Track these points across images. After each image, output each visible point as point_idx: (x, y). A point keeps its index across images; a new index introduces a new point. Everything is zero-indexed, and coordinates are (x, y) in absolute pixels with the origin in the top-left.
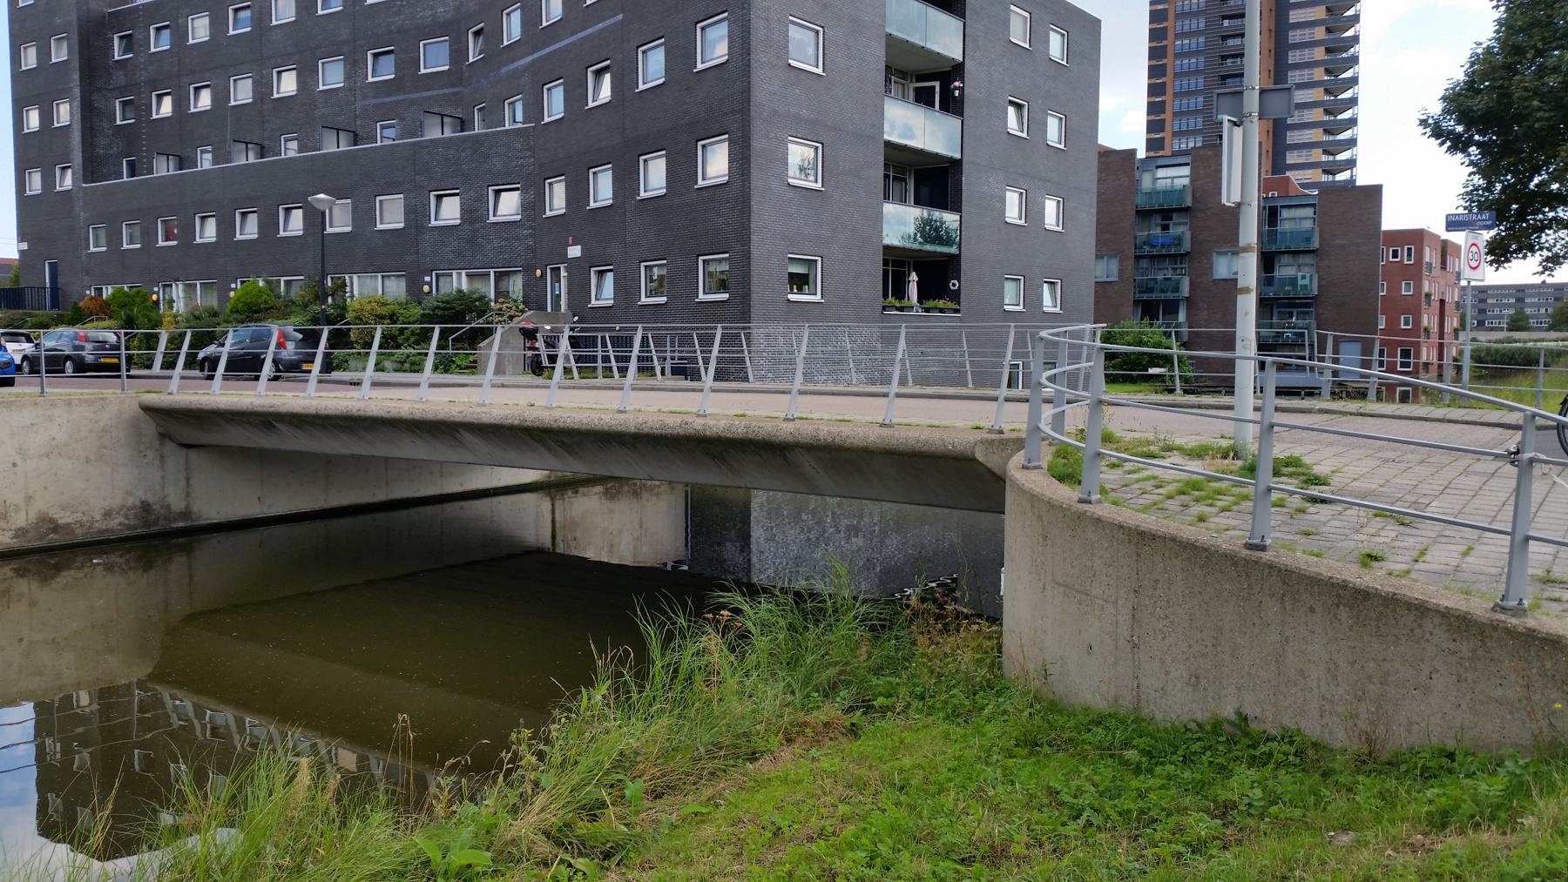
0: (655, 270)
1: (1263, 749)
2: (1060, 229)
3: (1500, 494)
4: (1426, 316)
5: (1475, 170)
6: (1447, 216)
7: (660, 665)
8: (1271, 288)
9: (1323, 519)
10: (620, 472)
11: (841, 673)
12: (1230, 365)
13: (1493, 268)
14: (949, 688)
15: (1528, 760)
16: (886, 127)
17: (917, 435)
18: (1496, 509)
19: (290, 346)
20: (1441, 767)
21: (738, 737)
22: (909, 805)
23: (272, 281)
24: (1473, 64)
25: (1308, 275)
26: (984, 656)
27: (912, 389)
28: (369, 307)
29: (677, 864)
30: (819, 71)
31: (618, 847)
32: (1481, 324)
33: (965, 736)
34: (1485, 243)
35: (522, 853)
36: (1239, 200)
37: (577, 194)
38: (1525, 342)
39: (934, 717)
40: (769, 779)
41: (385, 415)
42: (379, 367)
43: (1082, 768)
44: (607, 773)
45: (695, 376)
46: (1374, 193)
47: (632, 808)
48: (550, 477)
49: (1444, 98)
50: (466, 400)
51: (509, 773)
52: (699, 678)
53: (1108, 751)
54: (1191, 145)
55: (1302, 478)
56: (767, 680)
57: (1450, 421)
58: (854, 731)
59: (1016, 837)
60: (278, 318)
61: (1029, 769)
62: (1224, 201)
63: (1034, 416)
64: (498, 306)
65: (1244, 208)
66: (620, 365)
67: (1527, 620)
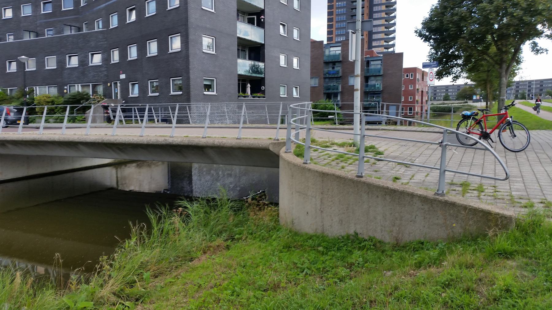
0: (155, 83)
1: (363, 244)
2: (298, 68)
3: (438, 156)
4: (417, 96)
5: (432, 47)
6: (423, 63)
7: (156, 229)
8: (367, 88)
9: (381, 166)
10: (142, 158)
11: (223, 227)
12: (352, 115)
13: (438, 80)
14: (261, 230)
15: (445, 243)
16: (238, 32)
17: (249, 142)
18: (437, 161)
19: (12, 114)
20: (419, 247)
21: (186, 253)
22: (246, 272)
23: (4, 90)
24: (431, 12)
25: (379, 84)
26: (273, 218)
27: (248, 125)
28: (43, 99)
29: (163, 301)
30: (213, 11)
31: (141, 297)
32: (435, 98)
33: (266, 246)
34: (435, 72)
35: (105, 301)
36: (354, 59)
37: (124, 55)
38: (448, 104)
39: (256, 240)
40: (197, 267)
41: (49, 140)
42: (47, 121)
43: (305, 255)
44: (136, 270)
45: (171, 122)
46: (401, 55)
47: (146, 282)
48: (115, 161)
49: (422, 23)
50: (80, 133)
51: (99, 272)
52: (171, 233)
53: (313, 248)
54: (342, 39)
55: (375, 152)
56: (197, 232)
57: (423, 132)
58: (228, 248)
59: (282, 281)
60: (8, 104)
61: (287, 256)
62: (350, 59)
63: (289, 134)
64: (93, 97)
65: (356, 62)
66: (141, 118)
67: (445, 198)
